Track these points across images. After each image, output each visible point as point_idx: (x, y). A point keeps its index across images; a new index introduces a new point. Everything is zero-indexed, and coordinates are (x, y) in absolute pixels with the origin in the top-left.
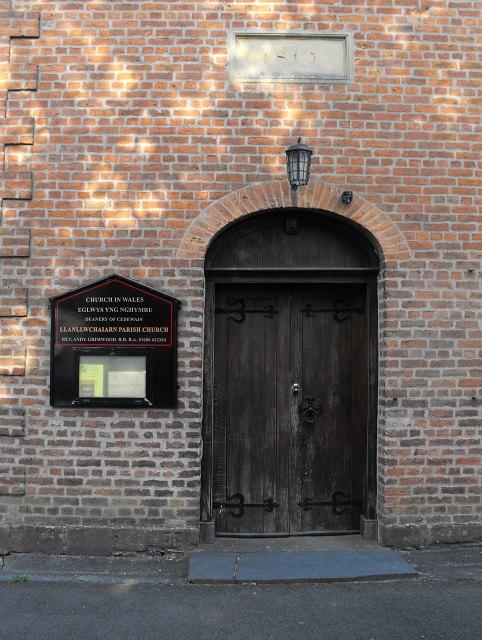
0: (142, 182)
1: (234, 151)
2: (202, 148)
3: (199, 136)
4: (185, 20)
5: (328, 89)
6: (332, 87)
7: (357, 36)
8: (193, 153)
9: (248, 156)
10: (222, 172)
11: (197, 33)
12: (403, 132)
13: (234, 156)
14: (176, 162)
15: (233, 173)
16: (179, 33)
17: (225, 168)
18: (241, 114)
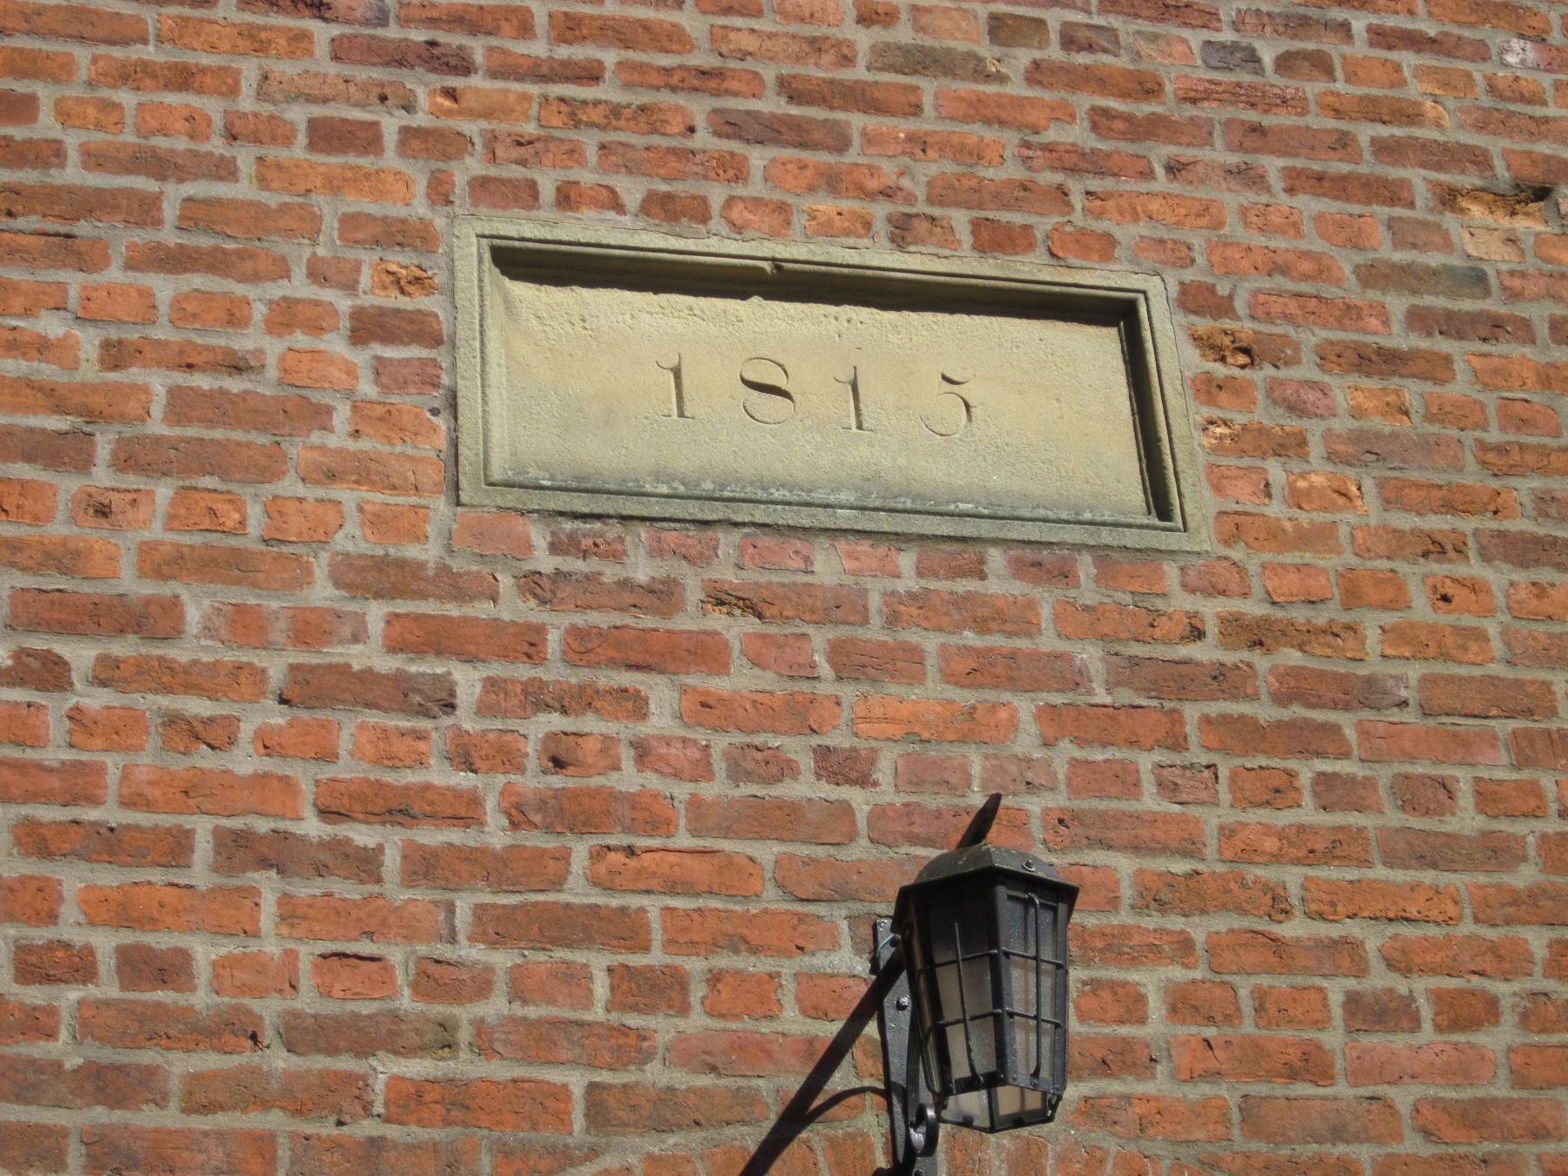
0: (392, 1132)
1: (497, 928)
2: (285, 899)
3: (262, 826)
4: (182, 144)
5: (1065, 575)
6: (1085, 567)
7: (1193, 300)
8: (222, 931)
9: (598, 962)
10: (416, 1068)
11: (257, 218)
12: (1526, 830)
13: (502, 960)
14: (108, 988)
15: (499, 1070)
16: (145, 211)
17: (444, 1040)
18: (537, 699)
